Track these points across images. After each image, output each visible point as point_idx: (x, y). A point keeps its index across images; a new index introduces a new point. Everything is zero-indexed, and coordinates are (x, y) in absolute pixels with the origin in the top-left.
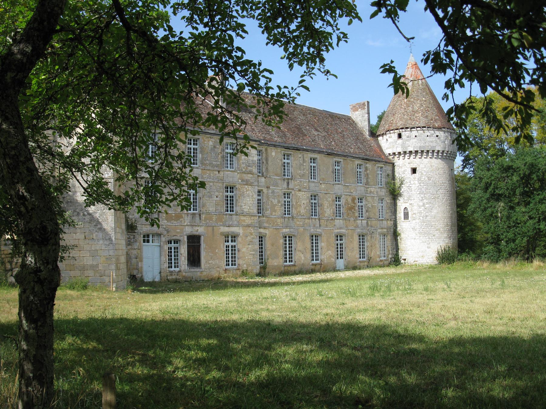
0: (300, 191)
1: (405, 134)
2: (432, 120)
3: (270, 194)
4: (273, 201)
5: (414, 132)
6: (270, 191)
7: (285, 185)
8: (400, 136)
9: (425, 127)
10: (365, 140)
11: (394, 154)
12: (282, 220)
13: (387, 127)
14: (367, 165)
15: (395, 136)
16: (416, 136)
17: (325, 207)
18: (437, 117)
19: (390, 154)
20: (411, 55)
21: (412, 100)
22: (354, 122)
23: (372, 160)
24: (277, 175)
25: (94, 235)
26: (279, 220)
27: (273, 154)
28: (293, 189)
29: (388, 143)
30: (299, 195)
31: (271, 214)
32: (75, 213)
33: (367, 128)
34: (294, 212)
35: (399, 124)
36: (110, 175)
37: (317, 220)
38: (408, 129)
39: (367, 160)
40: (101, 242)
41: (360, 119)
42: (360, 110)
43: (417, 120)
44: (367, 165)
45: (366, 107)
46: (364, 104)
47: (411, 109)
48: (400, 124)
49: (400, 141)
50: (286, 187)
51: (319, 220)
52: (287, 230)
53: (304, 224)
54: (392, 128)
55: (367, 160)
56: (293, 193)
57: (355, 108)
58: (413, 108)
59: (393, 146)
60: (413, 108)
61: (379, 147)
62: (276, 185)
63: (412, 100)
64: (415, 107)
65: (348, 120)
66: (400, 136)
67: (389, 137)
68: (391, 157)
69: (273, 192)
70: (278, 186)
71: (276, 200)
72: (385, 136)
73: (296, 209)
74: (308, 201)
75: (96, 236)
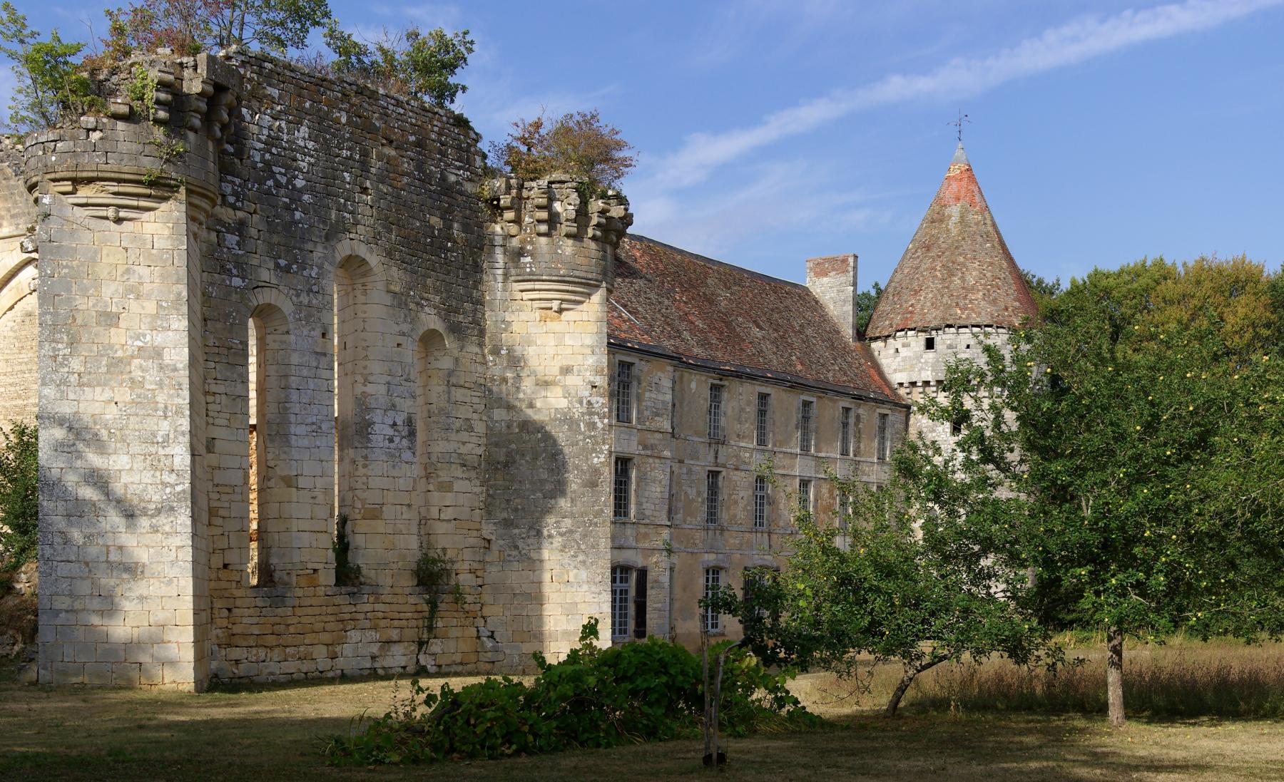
0: (737, 469)
1: (941, 339)
2: (1006, 309)
3: (685, 477)
4: (689, 491)
5: (967, 336)
6: (684, 471)
7: (711, 458)
8: (930, 344)
9: (990, 326)
10: (846, 350)
11: (913, 384)
12: (703, 533)
13: (898, 319)
14: (861, 411)
15: (917, 341)
16: (968, 347)
17: (781, 506)
18: (1017, 304)
19: (901, 384)
20: (960, 145)
21: (961, 259)
22: (817, 302)
23: (868, 399)
24: (697, 433)
25: (571, 574)
26: (698, 535)
27: (693, 385)
28: (724, 466)
29: (899, 359)
30: (735, 478)
31: (685, 521)
32: (533, 533)
33: (851, 319)
34: (724, 516)
35: (929, 317)
36: (602, 460)
37: (766, 535)
38: (953, 330)
39: (859, 398)
40: (585, 587)
41: (834, 296)
42: (833, 274)
43: (972, 309)
44: (861, 411)
45: (850, 269)
46: (844, 261)
47: (957, 281)
48: (933, 317)
49: (930, 355)
50: (713, 460)
51: (769, 533)
52: (712, 557)
53: (741, 544)
54: (913, 326)
55: (859, 398)
56: (724, 474)
57: (821, 269)
58: (963, 279)
59: (912, 367)
60: (963, 279)
61: (877, 367)
62: (694, 456)
63: (961, 259)
64: (968, 278)
65: (802, 294)
66: (930, 344)
67: (904, 345)
68: (902, 391)
69: (689, 472)
70: (698, 459)
71: (694, 491)
72: (891, 341)
73: (728, 509)
74: (750, 492)
75: (576, 575)
